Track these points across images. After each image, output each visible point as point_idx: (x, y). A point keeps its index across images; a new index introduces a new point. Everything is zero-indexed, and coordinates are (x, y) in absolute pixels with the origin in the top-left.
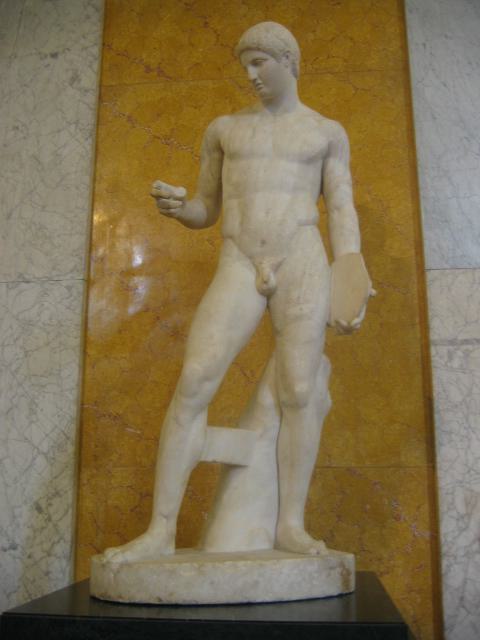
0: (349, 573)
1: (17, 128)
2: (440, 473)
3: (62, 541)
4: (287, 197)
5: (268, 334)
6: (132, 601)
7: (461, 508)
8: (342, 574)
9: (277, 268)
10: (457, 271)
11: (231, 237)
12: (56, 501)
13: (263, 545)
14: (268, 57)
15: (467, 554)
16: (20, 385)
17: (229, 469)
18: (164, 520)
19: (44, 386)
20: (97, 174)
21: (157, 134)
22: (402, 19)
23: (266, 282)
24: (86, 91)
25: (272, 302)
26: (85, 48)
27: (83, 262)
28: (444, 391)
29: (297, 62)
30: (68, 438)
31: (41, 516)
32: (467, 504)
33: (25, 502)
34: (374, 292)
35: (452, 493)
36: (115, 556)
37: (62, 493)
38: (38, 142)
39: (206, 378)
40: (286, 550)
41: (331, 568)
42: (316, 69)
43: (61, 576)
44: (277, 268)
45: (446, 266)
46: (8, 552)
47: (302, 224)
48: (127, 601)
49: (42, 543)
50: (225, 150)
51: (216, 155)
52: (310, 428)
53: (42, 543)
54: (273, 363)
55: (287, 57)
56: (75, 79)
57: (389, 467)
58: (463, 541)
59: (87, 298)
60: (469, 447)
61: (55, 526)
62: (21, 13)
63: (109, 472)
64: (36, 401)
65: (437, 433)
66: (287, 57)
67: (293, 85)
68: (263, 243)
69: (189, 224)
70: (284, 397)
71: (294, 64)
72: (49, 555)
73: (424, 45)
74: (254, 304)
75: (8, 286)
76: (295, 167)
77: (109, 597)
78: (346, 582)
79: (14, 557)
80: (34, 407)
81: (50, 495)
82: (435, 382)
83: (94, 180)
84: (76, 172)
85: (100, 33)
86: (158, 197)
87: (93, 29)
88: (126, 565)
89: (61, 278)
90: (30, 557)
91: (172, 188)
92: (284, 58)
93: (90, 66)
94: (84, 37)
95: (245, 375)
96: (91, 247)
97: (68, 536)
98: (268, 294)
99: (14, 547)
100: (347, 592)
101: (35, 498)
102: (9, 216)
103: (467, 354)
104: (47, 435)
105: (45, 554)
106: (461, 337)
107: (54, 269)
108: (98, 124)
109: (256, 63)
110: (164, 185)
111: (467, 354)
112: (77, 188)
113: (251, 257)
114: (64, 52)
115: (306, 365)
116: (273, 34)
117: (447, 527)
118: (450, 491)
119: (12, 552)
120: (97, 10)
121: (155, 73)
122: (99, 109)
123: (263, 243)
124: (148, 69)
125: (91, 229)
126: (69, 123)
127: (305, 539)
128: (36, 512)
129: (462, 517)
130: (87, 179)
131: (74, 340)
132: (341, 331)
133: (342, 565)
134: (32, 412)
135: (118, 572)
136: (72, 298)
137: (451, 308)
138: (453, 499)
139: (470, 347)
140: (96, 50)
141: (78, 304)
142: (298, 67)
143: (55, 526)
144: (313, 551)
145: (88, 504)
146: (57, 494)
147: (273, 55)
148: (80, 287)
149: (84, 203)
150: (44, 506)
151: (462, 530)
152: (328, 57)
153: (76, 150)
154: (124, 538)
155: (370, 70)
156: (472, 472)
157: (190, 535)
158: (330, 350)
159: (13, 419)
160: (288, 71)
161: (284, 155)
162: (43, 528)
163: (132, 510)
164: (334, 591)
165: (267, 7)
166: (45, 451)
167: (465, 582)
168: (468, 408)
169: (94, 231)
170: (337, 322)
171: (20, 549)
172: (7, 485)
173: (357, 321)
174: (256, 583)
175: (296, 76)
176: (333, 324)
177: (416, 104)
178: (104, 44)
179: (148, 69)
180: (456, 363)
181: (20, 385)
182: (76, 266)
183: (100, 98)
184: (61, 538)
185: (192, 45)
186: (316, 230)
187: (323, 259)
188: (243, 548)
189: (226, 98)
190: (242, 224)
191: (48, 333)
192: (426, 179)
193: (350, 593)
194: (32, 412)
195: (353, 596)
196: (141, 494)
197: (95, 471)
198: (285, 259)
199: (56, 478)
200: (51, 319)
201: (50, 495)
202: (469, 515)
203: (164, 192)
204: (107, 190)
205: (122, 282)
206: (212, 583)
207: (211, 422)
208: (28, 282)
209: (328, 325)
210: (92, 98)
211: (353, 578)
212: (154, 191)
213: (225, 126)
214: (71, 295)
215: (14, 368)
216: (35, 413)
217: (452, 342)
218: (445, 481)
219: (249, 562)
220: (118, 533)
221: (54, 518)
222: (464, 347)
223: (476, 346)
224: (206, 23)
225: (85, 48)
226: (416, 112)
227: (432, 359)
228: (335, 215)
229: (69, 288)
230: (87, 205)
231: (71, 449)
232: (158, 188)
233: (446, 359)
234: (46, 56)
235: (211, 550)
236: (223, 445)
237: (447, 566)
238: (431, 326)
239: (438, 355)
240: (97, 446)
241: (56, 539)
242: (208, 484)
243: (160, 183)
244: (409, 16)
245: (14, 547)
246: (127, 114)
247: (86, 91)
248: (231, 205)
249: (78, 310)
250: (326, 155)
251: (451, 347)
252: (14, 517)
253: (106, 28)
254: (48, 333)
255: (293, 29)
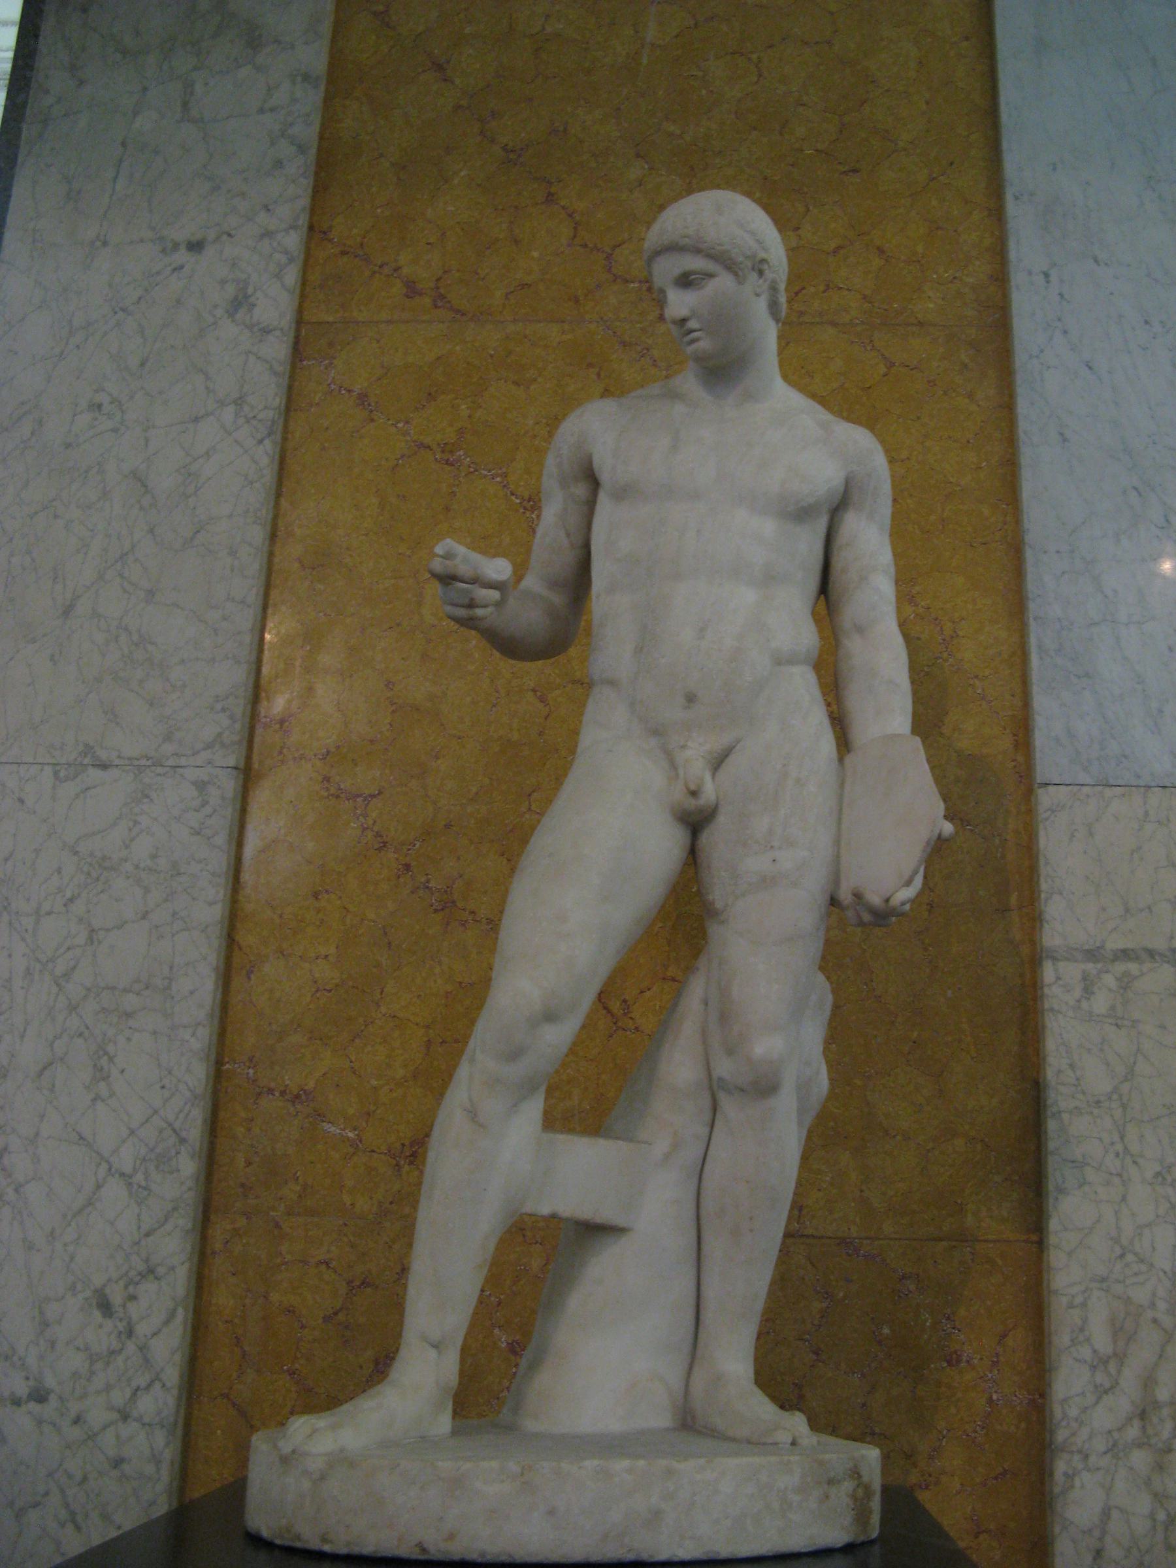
0: (868, 1493)
1: (100, 406)
2: (1056, 1257)
3: (157, 1385)
4: (748, 596)
5: (683, 921)
6: (356, 1550)
7: (1102, 1340)
8: (853, 1497)
9: (718, 762)
10: (1108, 792)
11: (612, 683)
12: (148, 1289)
13: (660, 1419)
14: (711, 266)
15: (1113, 1449)
16: (73, 1008)
17: (593, 1231)
18: (433, 1353)
19: (129, 1015)
20: (281, 524)
21: (428, 440)
22: (998, 214)
23: (694, 794)
24: (266, 331)
25: (704, 839)
26: (267, 234)
27: (238, 726)
28: (1072, 1066)
29: (782, 286)
30: (183, 1141)
31: (109, 1324)
32: (1117, 1329)
33: (73, 1288)
34: (948, 828)
35: (1084, 1305)
36: (316, 1437)
37: (161, 1270)
38: (147, 440)
39: (550, 1016)
40: (711, 1433)
41: (830, 1482)
42: (801, 313)
43: (150, 1469)
44: (718, 762)
45: (1083, 777)
46: (24, 1408)
47: (781, 660)
48: (343, 1550)
49: (108, 1388)
50: (605, 477)
51: (580, 490)
52: (770, 1150)
53: (108, 1388)
54: (696, 990)
55: (761, 273)
56: (240, 302)
57: (941, 1240)
58: (1103, 1418)
59: (243, 811)
60: (1124, 1199)
61: (143, 1348)
62: (123, 144)
63: (277, 1226)
64: (110, 1048)
65: (1052, 1163)
66: (761, 273)
67: (768, 335)
68: (691, 699)
69: (510, 647)
70: (724, 1067)
71: (773, 289)
72: (125, 1417)
73: (1047, 275)
74: (661, 847)
75: (56, 773)
76: (768, 527)
77: (298, 1537)
78: (861, 1517)
79: (40, 1422)
80: (104, 1061)
81: (132, 1273)
82: (1051, 1044)
83: (273, 536)
84: (230, 516)
85: (305, 201)
86: (448, 579)
87: (290, 194)
88: (341, 1460)
89: (183, 761)
90: (77, 1421)
91: (475, 557)
92: (755, 275)
93: (278, 276)
94: (267, 208)
95: (609, 1012)
96: (257, 692)
97: (173, 1375)
98: (695, 823)
99: (40, 1396)
100: (862, 1538)
101: (98, 1280)
102: (68, 611)
103: (1126, 983)
104: (132, 1132)
105: (115, 1416)
106: (1115, 943)
107: (168, 738)
108: (288, 409)
109: (686, 281)
110: (461, 550)
111: (1126, 983)
112: (233, 553)
113: (657, 732)
114: (217, 239)
115: (770, 993)
116: (735, 218)
117: (1070, 1383)
118: (1079, 1300)
119: (33, 1406)
120: (302, 149)
121: (427, 301)
122: (292, 378)
123: (691, 699)
124: (412, 290)
125: (261, 651)
126: (222, 404)
127: (763, 1408)
128: (97, 1314)
129: (1105, 1362)
130: (258, 535)
131: (208, 910)
132: (867, 917)
133: (855, 1473)
134: (100, 1075)
135: (323, 1478)
136: (208, 810)
137: (1090, 876)
138: (1085, 1320)
139: (1133, 967)
140: (293, 241)
141: (221, 824)
142: (783, 299)
143: (143, 1348)
144: (784, 1437)
145: (223, 1299)
146: (150, 1272)
147: (730, 265)
148: (229, 785)
149: (248, 588)
150: (116, 1298)
151: (1101, 1392)
152: (827, 288)
153: (233, 468)
154: (324, 1396)
155: (921, 324)
156: (1130, 1258)
157: (491, 1387)
158: (833, 960)
159: (52, 1090)
160: (761, 306)
161: (726, 507)
162: (113, 1353)
163: (326, 1319)
164: (836, 1534)
165: (692, 169)
166: (128, 1169)
167: (1106, 1513)
168: (1124, 1107)
169: (267, 654)
170: (858, 896)
171: (53, 1399)
172: (30, 1247)
173: (906, 894)
174: (657, 1515)
175: (777, 321)
176: (845, 896)
177: (1023, 407)
178: (311, 228)
179: (412, 290)
180: (1100, 1003)
181: (73, 1008)
182: (220, 735)
183: (298, 351)
184: (157, 1378)
185: (516, 242)
186: (812, 677)
187: (827, 744)
188: (615, 1426)
189: (590, 365)
190: (639, 650)
191: (147, 890)
192: (1046, 578)
193: (872, 1542)
194: (100, 1075)
195: (876, 1549)
196: (349, 1283)
197: (242, 1222)
198: (738, 741)
199: (147, 1235)
200: (154, 857)
201: (132, 1273)
202: (1120, 1357)
203: (463, 570)
204: (300, 560)
205: (327, 779)
206: (551, 1512)
207: (553, 1122)
208: (104, 767)
209: (834, 901)
210: (278, 349)
211: (876, 1504)
212: (437, 565)
213: (598, 428)
214: (205, 804)
215: (60, 970)
216: (106, 1078)
217: (1092, 954)
218: (1067, 1274)
219: (641, 1463)
220: (292, 1373)
221: (142, 1329)
222: (1120, 967)
223: (1147, 966)
224: (550, 194)
225: (267, 234)
226: (1022, 425)
227: (1046, 990)
228: (854, 645)
229: (201, 786)
230: (253, 596)
231: (188, 1166)
232: (449, 556)
233: (1077, 993)
234: (176, 246)
235: (530, 1425)
236: (581, 1176)
237: (1066, 1474)
238: (1047, 917)
239: (1060, 983)
240: (249, 1163)
241: (142, 1381)
242: (540, 1259)
243: (446, 545)
244: (1012, 208)
245: (40, 1396)
246: (357, 388)
247: (266, 331)
248: (609, 601)
249: (221, 840)
250: (839, 507)
251: (1090, 966)
252: (46, 1324)
253: (320, 190)
254: (147, 890)
255: (769, 197)
